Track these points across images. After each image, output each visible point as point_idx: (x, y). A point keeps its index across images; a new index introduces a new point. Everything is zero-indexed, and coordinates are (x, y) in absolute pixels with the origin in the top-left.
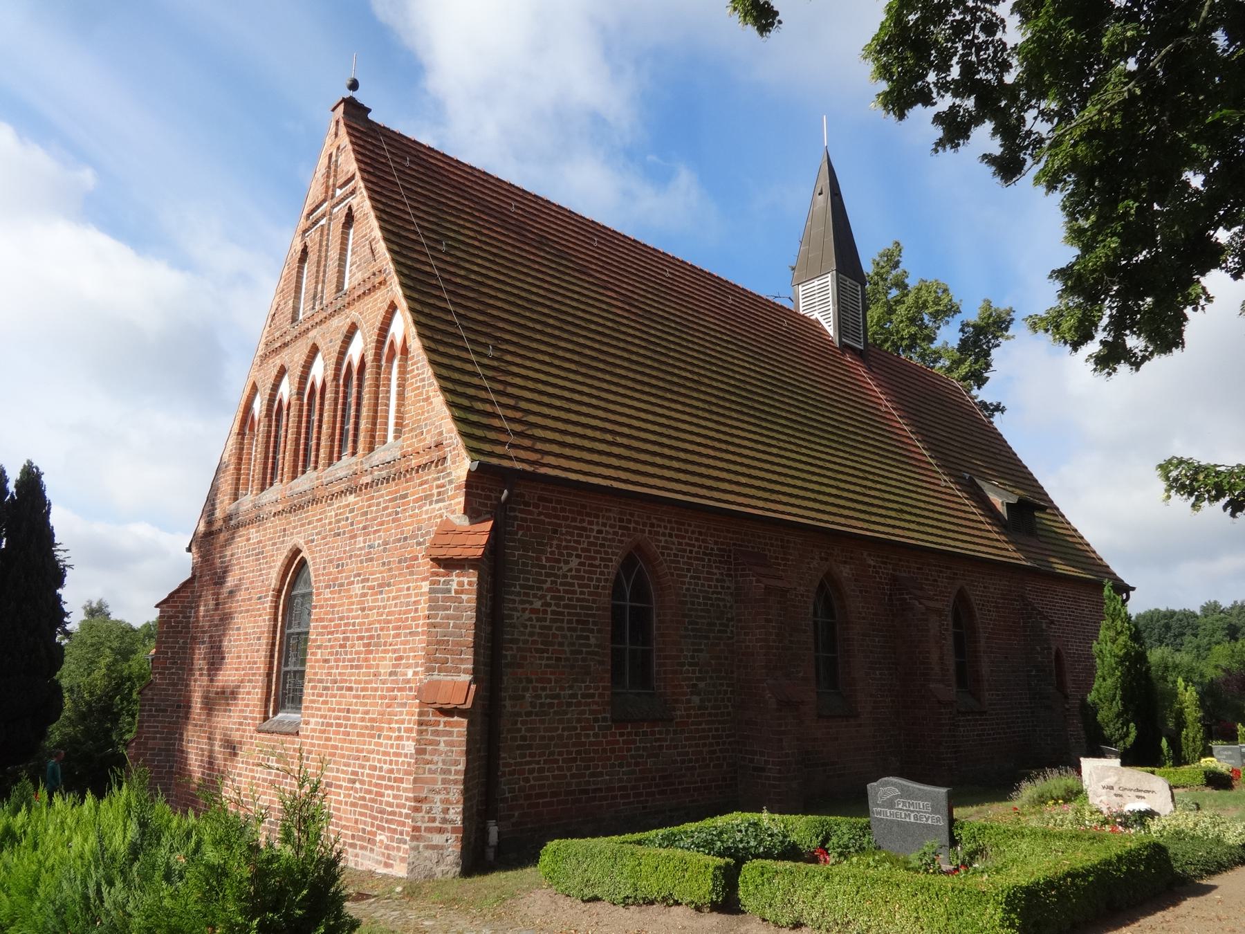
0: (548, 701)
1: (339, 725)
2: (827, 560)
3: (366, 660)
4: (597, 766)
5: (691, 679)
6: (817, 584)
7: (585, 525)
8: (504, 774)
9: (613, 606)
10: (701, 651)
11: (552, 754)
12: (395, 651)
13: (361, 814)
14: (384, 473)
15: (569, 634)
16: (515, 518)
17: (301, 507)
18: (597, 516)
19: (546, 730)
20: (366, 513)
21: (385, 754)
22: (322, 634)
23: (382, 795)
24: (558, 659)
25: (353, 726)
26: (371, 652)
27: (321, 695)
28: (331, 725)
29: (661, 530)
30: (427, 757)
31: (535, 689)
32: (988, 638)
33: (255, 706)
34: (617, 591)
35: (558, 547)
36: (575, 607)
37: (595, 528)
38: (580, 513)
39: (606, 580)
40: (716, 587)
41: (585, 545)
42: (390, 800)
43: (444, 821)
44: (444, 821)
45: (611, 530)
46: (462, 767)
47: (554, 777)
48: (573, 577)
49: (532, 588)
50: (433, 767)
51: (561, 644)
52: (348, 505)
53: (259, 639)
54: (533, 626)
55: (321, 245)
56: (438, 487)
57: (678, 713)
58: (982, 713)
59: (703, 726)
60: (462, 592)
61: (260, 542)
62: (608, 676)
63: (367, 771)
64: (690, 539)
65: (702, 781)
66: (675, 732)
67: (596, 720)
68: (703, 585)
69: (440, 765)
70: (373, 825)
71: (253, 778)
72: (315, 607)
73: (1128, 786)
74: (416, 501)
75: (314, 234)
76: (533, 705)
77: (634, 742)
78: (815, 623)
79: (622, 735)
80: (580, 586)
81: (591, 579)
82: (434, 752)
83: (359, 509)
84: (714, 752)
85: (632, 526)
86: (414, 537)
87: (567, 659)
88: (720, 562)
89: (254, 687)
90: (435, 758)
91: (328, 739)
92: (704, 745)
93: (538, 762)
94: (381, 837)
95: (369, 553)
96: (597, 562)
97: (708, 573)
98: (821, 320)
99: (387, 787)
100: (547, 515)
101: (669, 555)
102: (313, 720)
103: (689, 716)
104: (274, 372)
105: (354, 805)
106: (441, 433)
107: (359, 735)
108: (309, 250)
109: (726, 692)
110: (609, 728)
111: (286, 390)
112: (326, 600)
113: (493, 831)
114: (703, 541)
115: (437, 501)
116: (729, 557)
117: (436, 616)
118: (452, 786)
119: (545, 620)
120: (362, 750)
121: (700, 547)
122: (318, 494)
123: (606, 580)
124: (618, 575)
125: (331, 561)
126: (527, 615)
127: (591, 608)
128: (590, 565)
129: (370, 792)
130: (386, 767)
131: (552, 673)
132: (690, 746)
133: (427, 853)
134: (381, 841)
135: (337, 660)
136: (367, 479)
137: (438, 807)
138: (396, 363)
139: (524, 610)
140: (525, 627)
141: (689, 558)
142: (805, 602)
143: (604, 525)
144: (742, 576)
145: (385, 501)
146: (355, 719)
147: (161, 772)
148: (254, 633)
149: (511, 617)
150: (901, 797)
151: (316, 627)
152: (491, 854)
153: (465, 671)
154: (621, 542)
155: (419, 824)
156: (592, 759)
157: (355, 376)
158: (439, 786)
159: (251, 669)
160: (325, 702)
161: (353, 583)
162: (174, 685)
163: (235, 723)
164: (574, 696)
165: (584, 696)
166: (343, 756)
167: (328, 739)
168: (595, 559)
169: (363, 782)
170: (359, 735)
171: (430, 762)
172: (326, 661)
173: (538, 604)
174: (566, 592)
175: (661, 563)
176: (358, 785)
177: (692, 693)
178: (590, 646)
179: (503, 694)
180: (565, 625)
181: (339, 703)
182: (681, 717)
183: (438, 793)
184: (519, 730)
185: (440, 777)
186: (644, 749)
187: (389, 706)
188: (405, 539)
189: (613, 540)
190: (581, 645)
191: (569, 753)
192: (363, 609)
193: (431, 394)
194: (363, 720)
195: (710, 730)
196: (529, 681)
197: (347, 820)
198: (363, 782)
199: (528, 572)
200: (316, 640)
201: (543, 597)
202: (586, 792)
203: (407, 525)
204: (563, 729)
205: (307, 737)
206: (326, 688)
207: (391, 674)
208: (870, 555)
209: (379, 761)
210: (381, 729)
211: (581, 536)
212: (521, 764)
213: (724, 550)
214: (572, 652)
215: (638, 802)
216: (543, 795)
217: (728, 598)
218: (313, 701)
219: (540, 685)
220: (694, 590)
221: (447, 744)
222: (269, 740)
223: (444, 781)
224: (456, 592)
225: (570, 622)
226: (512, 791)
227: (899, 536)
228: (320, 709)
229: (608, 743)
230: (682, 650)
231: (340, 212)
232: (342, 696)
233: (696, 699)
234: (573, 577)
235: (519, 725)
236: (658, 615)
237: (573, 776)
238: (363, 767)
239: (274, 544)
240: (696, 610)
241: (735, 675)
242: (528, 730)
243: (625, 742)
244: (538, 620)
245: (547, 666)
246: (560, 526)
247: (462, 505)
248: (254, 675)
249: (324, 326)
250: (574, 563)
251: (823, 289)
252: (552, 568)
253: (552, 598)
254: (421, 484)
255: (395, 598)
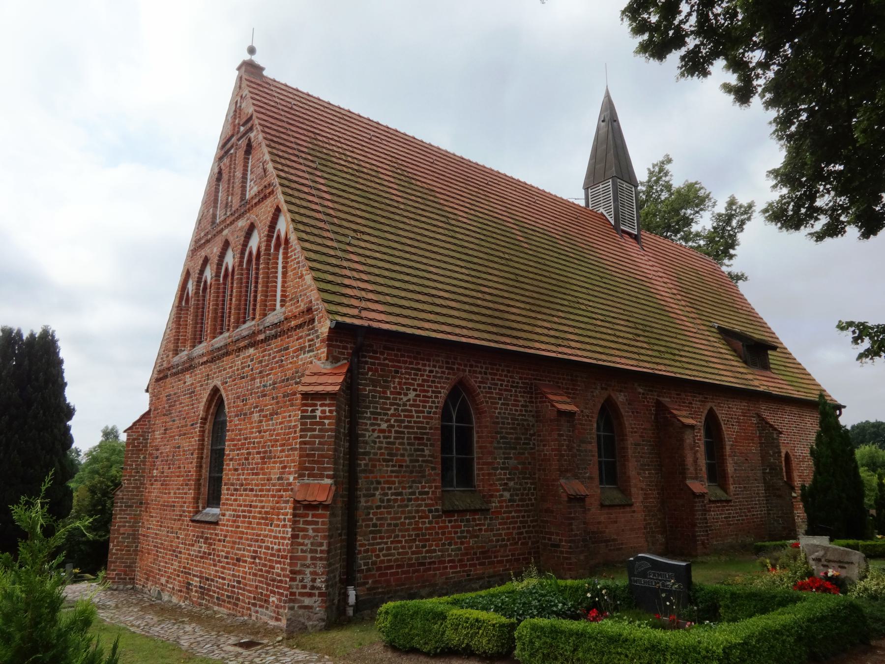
0: (393, 497)
1: (245, 517)
2: (606, 389)
3: (262, 469)
4: (431, 545)
5: (503, 480)
6: (599, 406)
7: (420, 367)
8: (360, 552)
9: (442, 426)
10: (511, 458)
11: (397, 536)
12: (281, 462)
13: (260, 582)
14: (273, 332)
15: (408, 447)
16: (366, 363)
17: (219, 359)
18: (429, 360)
19: (392, 519)
20: (261, 362)
21: (276, 537)
22: (233, 450)
23: (273, 568)
24: (401, 466)
25: (254, 517)
26: (265, 463)
27: (232, 495)
28: (239, 516)
29: (479, 370)
30: (300, 540)
31: (383, 489)
32: (732, 445)
33: (190, 503)
34: (446, 415)
35: (400, 383)
36: (412, 427)
37: (427, 368)
38: (415, 358)
39: (437, 407)
40: (521, 411)
41: (420, 382)
42: (279, 571)
43: (313, 588)
44: (313, 588)
45: (440, 370)
46: (324, 548)
47: (399, 554)
48: (411, 405)
49: (380, 414)
50: (305, 548)
51: (403, 455)
52: (249, 356)
53: (192, 454)
54: (381, 442)
55: (230, 168)
56: (309, 341)
57: (494, 505)
58: (728, 501)
59: (513, 514)
60: (325, 418)
61: (192, 384)
62: (438, 478)
63: (264, 550)
64: (501, 375)
65: (512, 555)
66: (491, 519)
67: (430, 511)
68: (511, 410)
69: (309, 546)
70: (267, 590)
71: (189, 555)
72: (228, 431)
73: (832, 558)
74: (294, 352)
75: (226, 161)
76: (382, 501)
77: (460, 527)
78: (599, 437)
79: (450, 522)
80: (417, 412)
81: (424, 407)
82: (304, 537)
83: (257, 359)
84: (522, 533)
85: (456, 367)
86: (293, 378)
87: (407, 466)
88: (524, 392)
89: (189, 489)
90: (306, 541)
91: (238, 527)
92: (514, 528)
93: (386, 543)
94: (273, 599)
95: (264, 391)
96: (430, 394)
97: (515, 400)
98: (605, 213)
99: (277, 562)
100: (390, 360)
101: (484, 388)
102: (228, 513)
103: (501, 507)
104: (201, 262)
105: (255, 575)
106: (311, 302)
107: (258, 524)
108: (223, 172)
109: (530, 489)
110: (439, 517)
111: (209, 274)
112: (236, 425)
113: (352, 594)
114: (511, 377)
115: (309, 352)
116: (531, 388)
117: (305, 436)
118: (318, 562)
119: (390, 437)
120: (259, 535)
121: (508, 381)
122: (230, 349)
123: (437, 407)
124: (446, 402)
125: (238, 398)
126: (376, 434)
127: (425, 428)
128: (424, 396)
129: (265, 565)
130: (276, 547)
131: (396, 477)
132: (503, 529)
133: (301, 612)
134: (273, 602)
135: (243, 469)
136: (261, 337)
137: (308, 578)
138: (281, 251)
139: (374, 431)
140: (375, 442)
141: (500, 390)
142: (590, 421)
143: (434, 366)
144: (540, 402)
145: (274, 353)
146: (255, 512)
147: (129, 551)
148: (189, 450)
149: (364, 436)
150: (652, 569)
151: (229, 446)
152: (350, 612)
153: (328, 477)
154: (447, 379)
155: (294, 590)
156: (428, 540)
157: (254, 262)
158: (309, 562)
159: (187, 476)
160: (236, 500)
161: (253, 412)
162: (138, 488)
163: (177, 515)
164: (413, 493)
165: (421, 493)
166: (247, 539)
167: (238, 527)
168: (428, 391)
169: (260, 558)
170: (258, 524)
171: (303, 544)
172: (236, 470)
173: (384, 426)
174: (405, 416)
175: (479, 394)
176: (257, 561)
177: (504, 490)
178: (425, 456)
179: (359, 493)
180: (405, 441)
181: (245, 501)
182: (496, 507)
183: (308, 567)
184: (372, 519)
185: (309, 556)
186: (468, 532)
187: (277, 502)
188: (288, 380)
189: (441, 378)
190: (418, 456)
191: (409, 536)
192: (260, 432)
193: (304, 273)
194: (260, 513)
195: (518, 517)
196: (379, 483)
197: (251, 586)
198: (260, 558)
199: (377, 402)
200: (229, 455)
201: (388, 421)
202: (423, 564)
203: (289, 369)
204: (405, 518)
205: (224, 525)
206: (236, 490)
207: (279, 479)
208: (639, 385)
209: (272, 543)
210: (272, 520)
211: (417, 375)
212: (373, 544)
213: (527, 383)
214: (411, 461)
215: (464, 571)
216: (391, 567)
217: (531, 419)
218: (227, 499)
219: (386, 486)
220: (505, 413)
221: (314, 530)
222: (199, 527)
223: (312, 558)
224: (320, 418)
225: (409, 438)
226: (366, 564)
227: (662, 370)
228: (232, 505)
229: (440, 528)
230: (495, 458)
231: (243, 143)
232: (247, 495)
233: (507, 495)
234: (411, 405)
235: (371, 516)
236: (477, 432)
237: (413, 553)
238: (260, 547)
239: (202, 386)
240: (507, 428)
241: (537, 476)
242: (378, 519)
243: (452, 527)
244: (385, 437)
245: (392, 472)
246: (401, 367)
247: (325, 354)
248: (189, 480)
249: (233, 226)
250: (412, 395)
251: (606, 191)
252: (395, 399)
253: (396, 421)
254: (298, 339)
255: (281, 423)
